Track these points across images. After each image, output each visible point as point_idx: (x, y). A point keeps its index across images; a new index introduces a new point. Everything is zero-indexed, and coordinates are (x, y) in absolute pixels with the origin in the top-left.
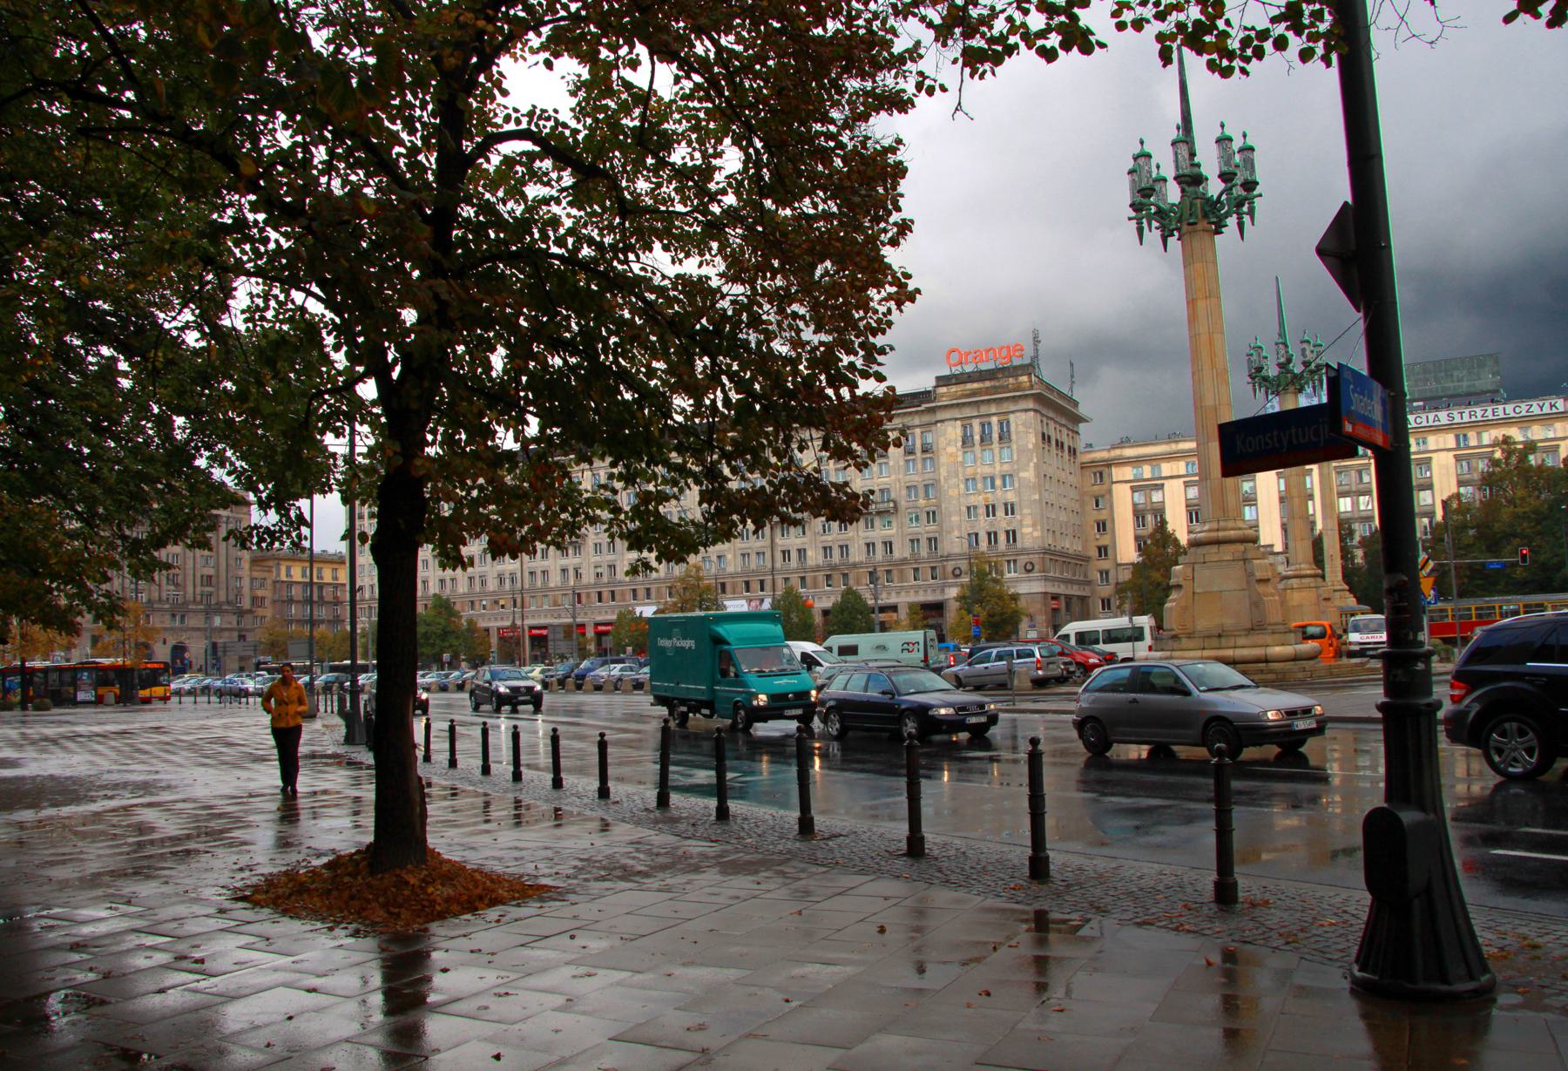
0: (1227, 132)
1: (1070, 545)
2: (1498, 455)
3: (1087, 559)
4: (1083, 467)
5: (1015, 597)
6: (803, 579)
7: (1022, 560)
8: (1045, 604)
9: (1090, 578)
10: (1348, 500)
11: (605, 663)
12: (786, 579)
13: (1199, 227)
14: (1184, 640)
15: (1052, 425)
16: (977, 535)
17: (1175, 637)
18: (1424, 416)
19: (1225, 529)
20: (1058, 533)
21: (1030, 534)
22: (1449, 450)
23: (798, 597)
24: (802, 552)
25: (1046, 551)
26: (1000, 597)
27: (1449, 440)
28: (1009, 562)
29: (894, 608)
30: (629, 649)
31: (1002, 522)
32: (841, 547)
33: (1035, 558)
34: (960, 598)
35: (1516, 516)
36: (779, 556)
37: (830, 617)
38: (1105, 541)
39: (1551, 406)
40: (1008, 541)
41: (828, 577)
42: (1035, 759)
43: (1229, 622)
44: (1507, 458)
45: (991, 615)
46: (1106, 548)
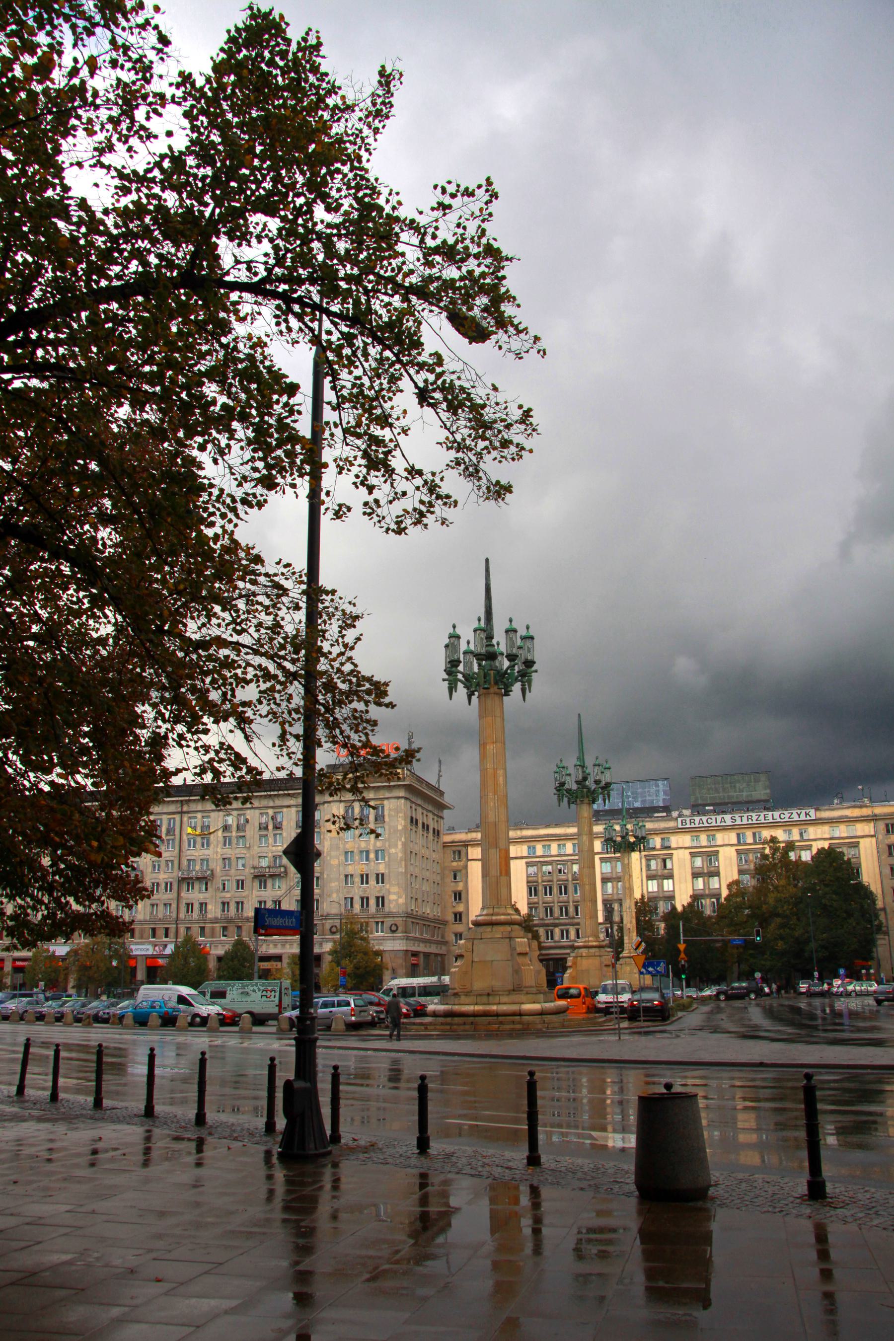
0: (515, 625)
1: (428, 910)
2: (767, 851)
3: (445, 923)
4: (445, 845)
5: (379, 953)
6: (203, 929)
7: (389, 921)
8: (405, 961)
9: (447, 939)
10: (655, 882)
11: (14, 996)
12: (188, 928)
13: (492, 690)
14: (463, 998)
15: (420, 810)
16: (352, 899)
17: (456, 995)
18: (713, 818)
19: (498, 914)
20: (420, 901)
21: (397, 900)
22: (732, 845)
23: (196, 944)
24: (203, 905)
25: (409, 916)
26: (366, 953)
27: (732, 837)
28: (377, 923)
29: (278, 958)
30: (42, 983)
31: (373, 889)
32: (238, 903)
33: (399, 921)
34: (333, 952)
35: (778, 900)
36: (183, 909)
37: (223, 963)
38: (461, 908)
39: (806, 814)
40: (378, 905)
41: (225, 928)
42: (423, 1090)
43: (497, 984)
44: (773, 854)
45: (357, 968)
46: (460, 914)
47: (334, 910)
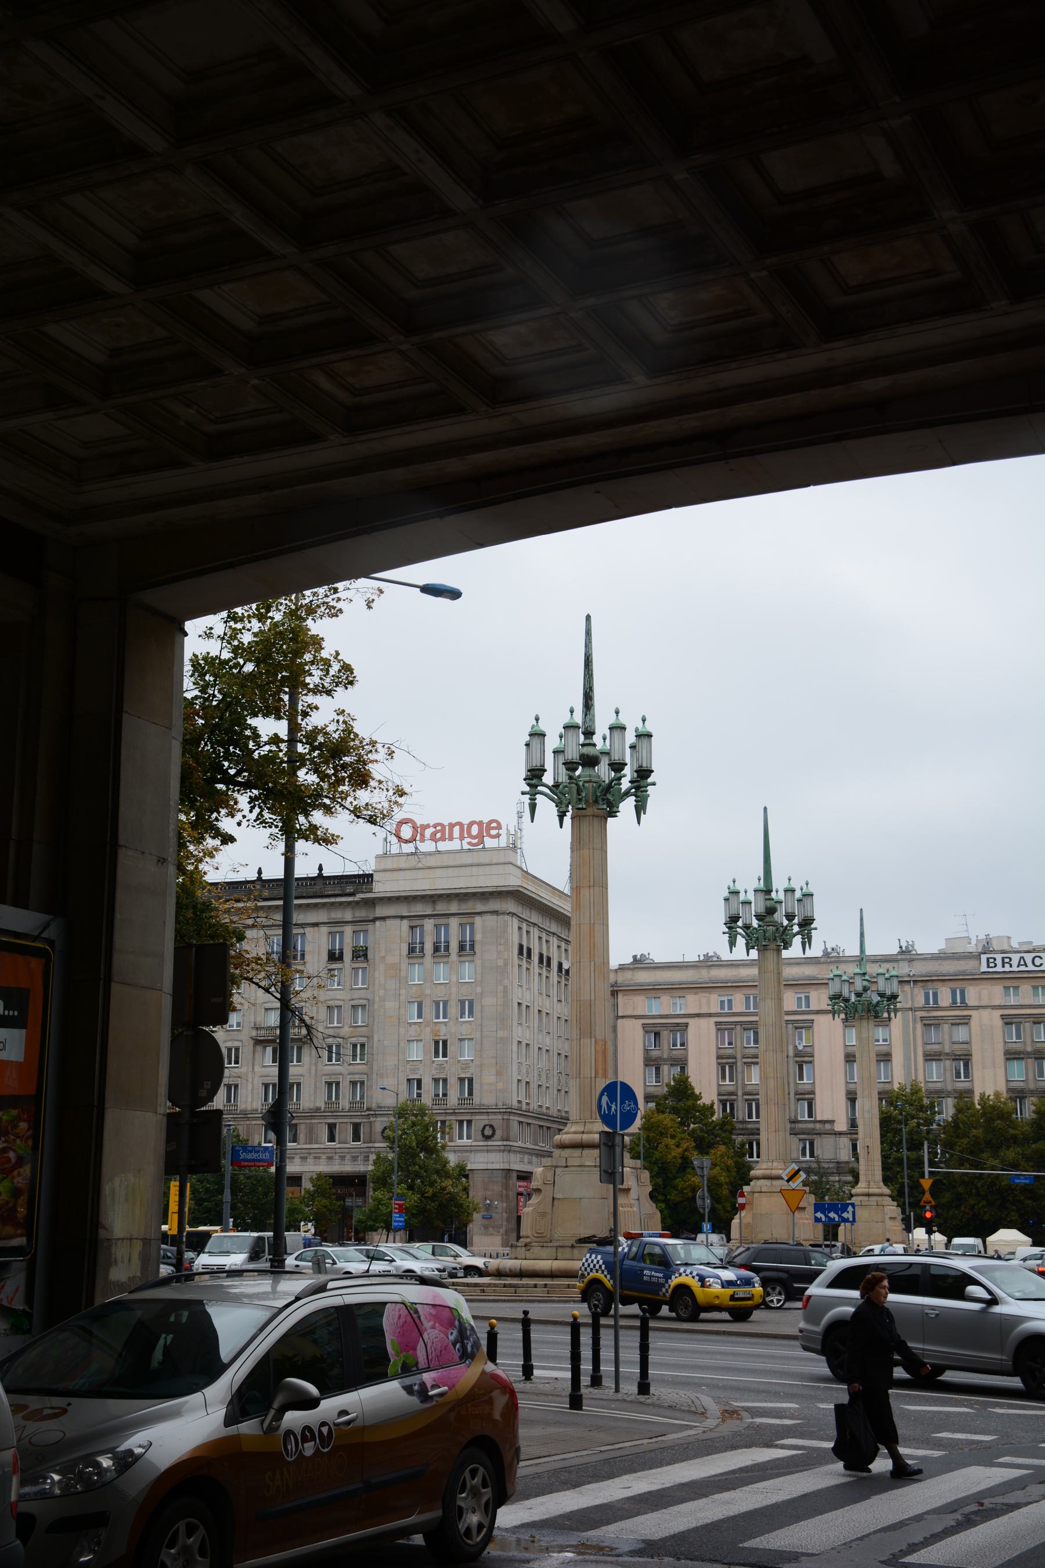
0: (623, 719)
7: (480, 1121)
15: (535, 933)
20: (534, 1086)
28: (461, 1122)
47: (390, 1101)
